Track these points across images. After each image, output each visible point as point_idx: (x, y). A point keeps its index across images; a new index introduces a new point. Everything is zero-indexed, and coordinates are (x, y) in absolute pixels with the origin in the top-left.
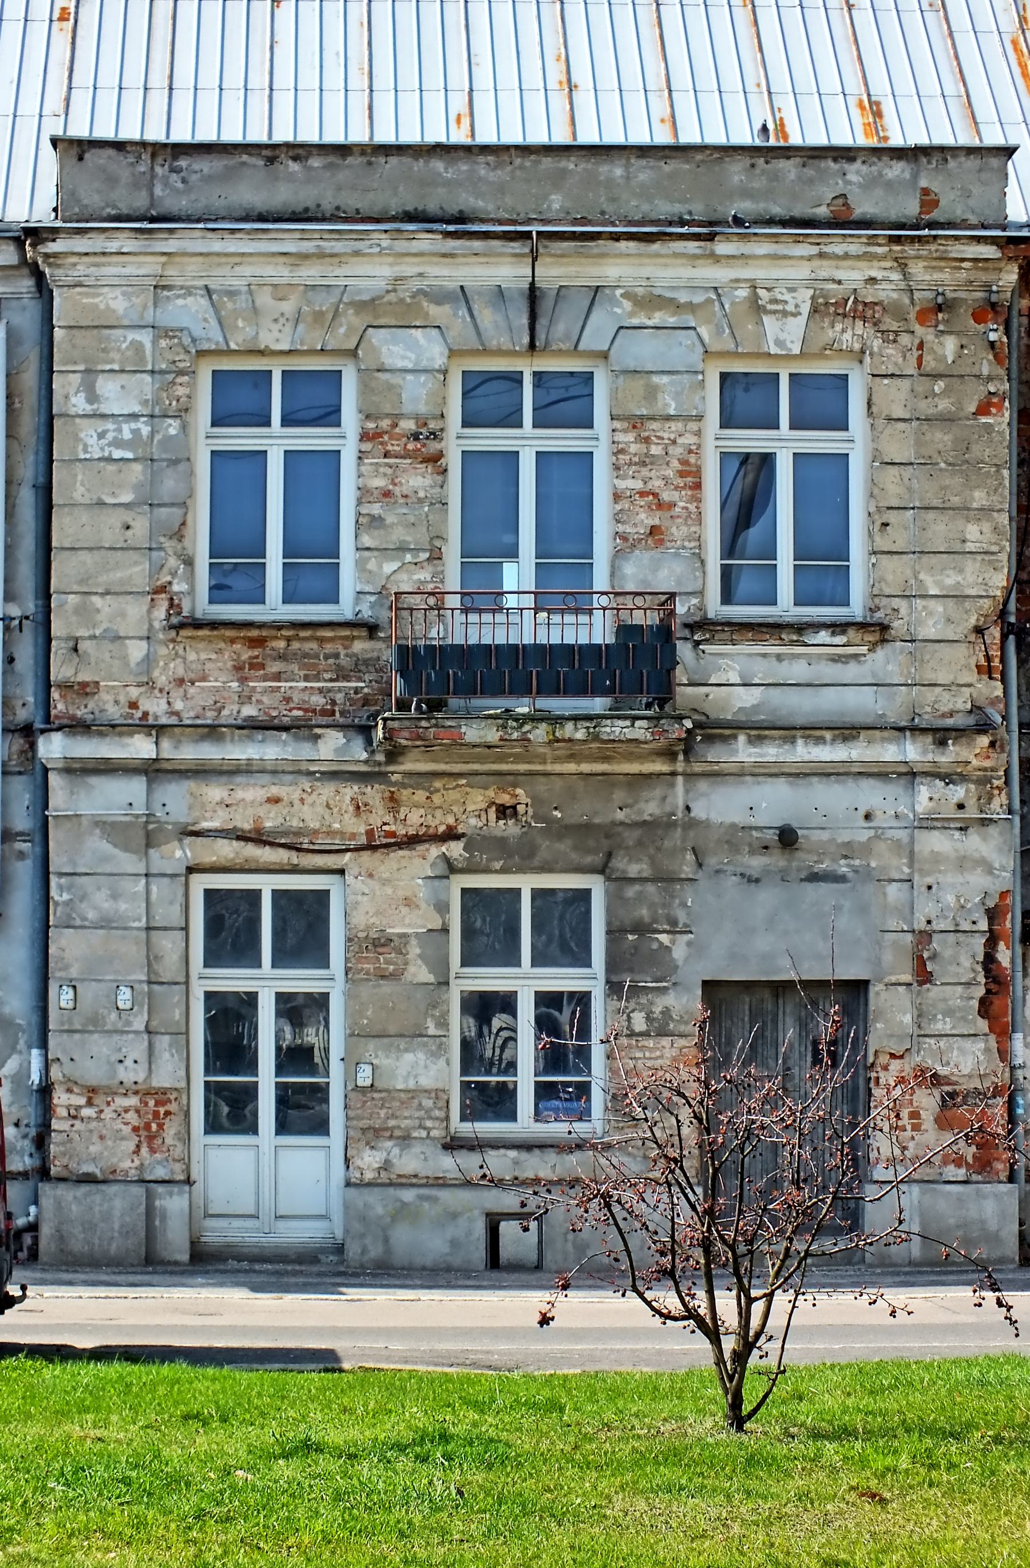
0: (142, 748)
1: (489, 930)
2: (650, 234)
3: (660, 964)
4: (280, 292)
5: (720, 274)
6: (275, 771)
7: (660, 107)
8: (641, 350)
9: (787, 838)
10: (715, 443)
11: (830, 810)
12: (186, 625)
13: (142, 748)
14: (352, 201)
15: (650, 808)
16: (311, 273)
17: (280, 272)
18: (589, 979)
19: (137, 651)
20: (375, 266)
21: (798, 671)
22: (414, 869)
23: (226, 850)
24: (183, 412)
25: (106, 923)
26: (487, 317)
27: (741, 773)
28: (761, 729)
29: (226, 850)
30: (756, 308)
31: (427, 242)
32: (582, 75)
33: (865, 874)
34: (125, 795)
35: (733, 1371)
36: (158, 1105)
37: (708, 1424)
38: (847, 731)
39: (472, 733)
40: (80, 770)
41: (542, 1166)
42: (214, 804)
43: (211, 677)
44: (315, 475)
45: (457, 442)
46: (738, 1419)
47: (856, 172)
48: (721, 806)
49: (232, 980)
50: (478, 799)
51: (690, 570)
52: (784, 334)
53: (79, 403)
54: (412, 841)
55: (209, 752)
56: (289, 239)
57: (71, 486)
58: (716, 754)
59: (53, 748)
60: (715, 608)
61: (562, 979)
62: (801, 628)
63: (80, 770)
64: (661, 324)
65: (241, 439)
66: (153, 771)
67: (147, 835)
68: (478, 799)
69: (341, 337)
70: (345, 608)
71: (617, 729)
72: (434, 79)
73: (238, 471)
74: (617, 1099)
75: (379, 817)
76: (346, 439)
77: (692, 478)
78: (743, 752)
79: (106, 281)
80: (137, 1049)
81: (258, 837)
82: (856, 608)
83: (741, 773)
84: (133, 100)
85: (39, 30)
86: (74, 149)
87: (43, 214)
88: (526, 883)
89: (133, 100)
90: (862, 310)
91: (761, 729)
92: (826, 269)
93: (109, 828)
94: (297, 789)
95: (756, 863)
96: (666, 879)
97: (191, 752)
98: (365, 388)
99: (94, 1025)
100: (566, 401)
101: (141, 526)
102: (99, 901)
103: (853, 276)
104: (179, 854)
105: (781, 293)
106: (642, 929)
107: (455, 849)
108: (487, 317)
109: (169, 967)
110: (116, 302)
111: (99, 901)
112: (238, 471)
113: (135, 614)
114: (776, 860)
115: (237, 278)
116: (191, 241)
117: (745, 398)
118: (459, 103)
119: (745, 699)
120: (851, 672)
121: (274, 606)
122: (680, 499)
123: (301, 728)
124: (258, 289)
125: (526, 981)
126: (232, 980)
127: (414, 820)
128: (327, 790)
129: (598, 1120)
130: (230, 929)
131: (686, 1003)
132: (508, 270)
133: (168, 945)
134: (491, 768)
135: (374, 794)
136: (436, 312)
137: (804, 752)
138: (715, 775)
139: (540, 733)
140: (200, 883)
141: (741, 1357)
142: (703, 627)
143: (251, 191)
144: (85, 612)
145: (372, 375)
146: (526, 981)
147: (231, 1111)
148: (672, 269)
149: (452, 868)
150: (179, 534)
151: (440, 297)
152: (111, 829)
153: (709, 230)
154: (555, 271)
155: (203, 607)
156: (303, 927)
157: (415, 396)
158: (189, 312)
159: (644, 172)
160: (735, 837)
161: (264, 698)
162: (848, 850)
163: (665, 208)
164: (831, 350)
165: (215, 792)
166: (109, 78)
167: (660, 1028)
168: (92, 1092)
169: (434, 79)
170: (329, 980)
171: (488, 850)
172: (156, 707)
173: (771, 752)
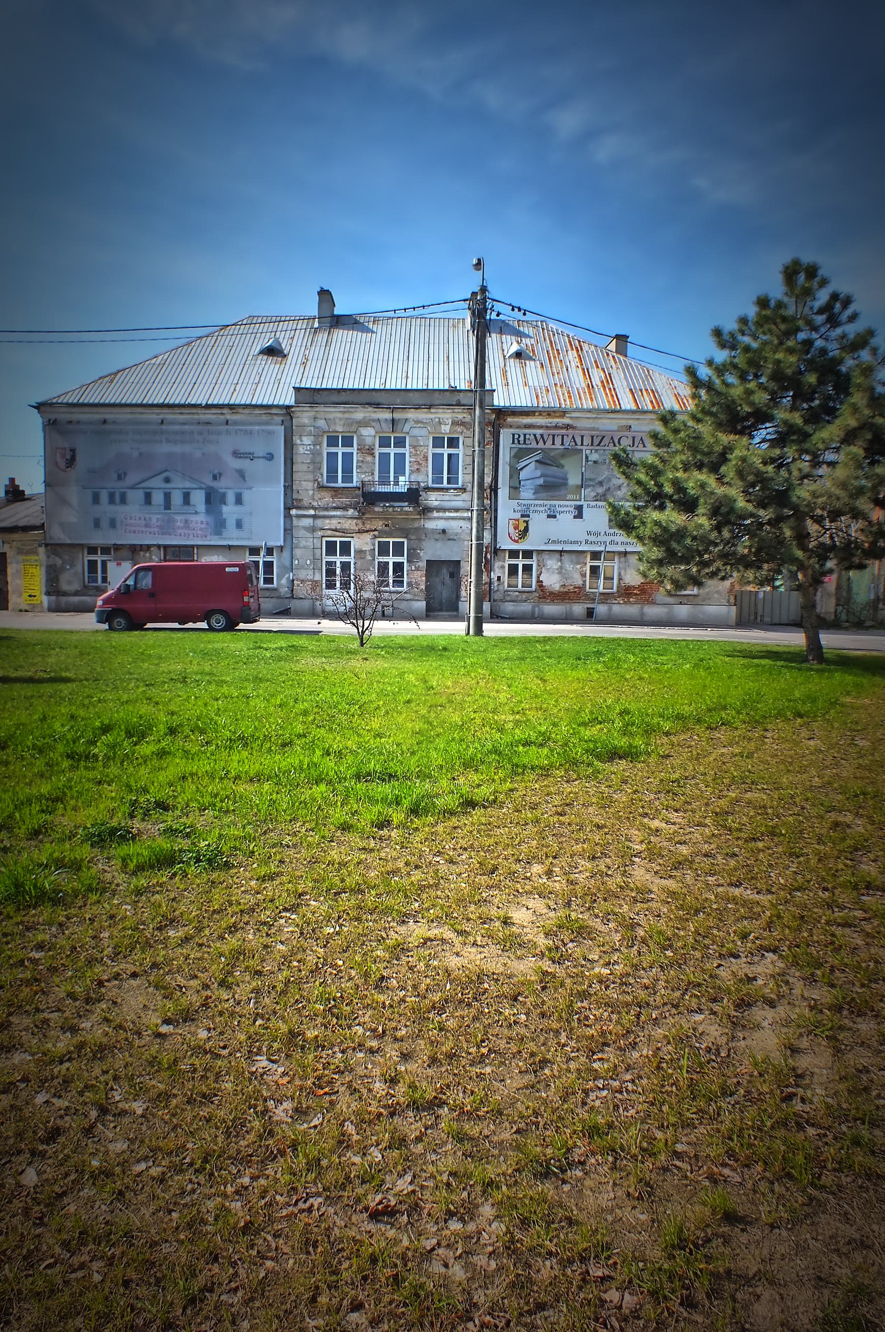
0: (312, 512)
1: (383, 549)
2: (418, 407)
3: (418, 557)
4: (340, 419)
5: (432, 416)
6: (339, 517)
7: (425, 382)
8: (416, 432)
9: (444, 531)
10: (431, 451)
11: (454, 526)
12: (321, 487)
13: (312, 512)
14: (355, 401)
15: (416, 525)
16: (346, 416)
17: (340, 415)
18: (403, 559)
19: (311, 492)
20: (360, 414)
21: (447, 498)
22: (367, 537)
23: (330, 533)
24: (320, 444)
25: (304, 547)
26: (383, 425)
27: (435, 518)
28: (439, 509)
29: (330, 533)
30: (440, 423)
31: (370, 409)
32: (410, 375)
33: (460, 539)
34: (308, 522)
35: (361, 635)
36: (315, 584)
37: (357, 643)
38: (457, 510)
39: (377, 509)
40: (299, 517)
41: (394, 597)
42: (327, 524)
43: (327, 499)
44: (348, 457)
45: (378, 451)
46: (362, 644)
47: (462, 394)
48: (431, 525)
49: (331, 559)
50: (381, 523)
51: (427, 478)
52: (446, 429)
53: (298, 442)
54: (367, 531)
55: (326, 513)
56: (341, 408)
57: (297, 459)
58: (430, 515)
59: (293, 512)
60: (430, 484)
61: (398, 559)
62: (448, 489)
63: (299, 517)
64: (420, 427)
65: (333, 450)
66: (314, 517)
67: (313, 529)
68: (381, 523)
69: (353, 428)
70: (355, 484)
71: (407, 509)
72: (379, 376)
73: (332, 457)
74: (410, 584)
75: (361, 526)
76: (354, 450)
77: (426, 458)
78: (435, 514)
79: (304, 417)
80: (311, 572)
81: (336, 530)
82: (460, 485)
83: (435, 518)
84: (315, 380)
85: (521, 388)
86: (297, 390)
87: (292, 403)
88: (391, 540)
89: (315, 380)
90: (462, 424)
91: (439, 509)
92: (454, 415)
93: (305, 528)
94: (346, 520)
95: (437, 536)
96: (419, 540)
97: (322, 513)
98: (358, 439)
99: (302, 568)
100: (400, 443)
101: (311, 468)
102: (303, 543)
103: (460, 416)
104: (320, 533)
105: (445, 420)
106: (414, 549)
107: (376, 533)
108: (383, 425)
109: (318, 555)
110: (306, 421)
111: (303, 543)
112: (332, 457)
113: (310, 485)
114: (442, 536)
115: (331, 416)
116: (321, 408)
117: (438, 442)
118: (383, 381)
119: (436, 503)
120: (458, 498)
121: (340, 484)
122: (424, 463)
123: (345, 508)
124: (336, 418)
125: (391, 560)
126: (331, 559)
127: (368, 527)
128: (350, 521)
129: (405, 588)
130: (331, 548)
131: (423, 564)
132: (387, 415)
133: (318, 552)
134: (383, 516)
135: (359, 522)
136: (373, 424)
137: (448, 514)
138: (430, 519)
139: (391, 509)
140: (325, 539)
141: (363, 632)
142: (427, 489)
143: (335, 398)
144: (300, 485)
145: (360, 436)
146: (391, 560)
147: (331, 585)
148: (422, 415)
149: (375, 537)
150: (320, 469)
151: (374, 421)
152: (305, 528)
153: (430, 407)
154: (397, 416)
155: (325, 483)
156: (346, 548)
157: (369, 441)
158: (321, 423)
159: (417, 395)
160: (434, 531)
161: (338, 501)
162: (457, 534)
163: (421, 402)
164: (455, 432)
165: (327, 521)
166: (311, 375)
167: (417, 569)
168: (302, 581)
169: (379, 376)
170: (351, 559)
171: (382, 534)
172: (315, 504)
173: (441, 514)
